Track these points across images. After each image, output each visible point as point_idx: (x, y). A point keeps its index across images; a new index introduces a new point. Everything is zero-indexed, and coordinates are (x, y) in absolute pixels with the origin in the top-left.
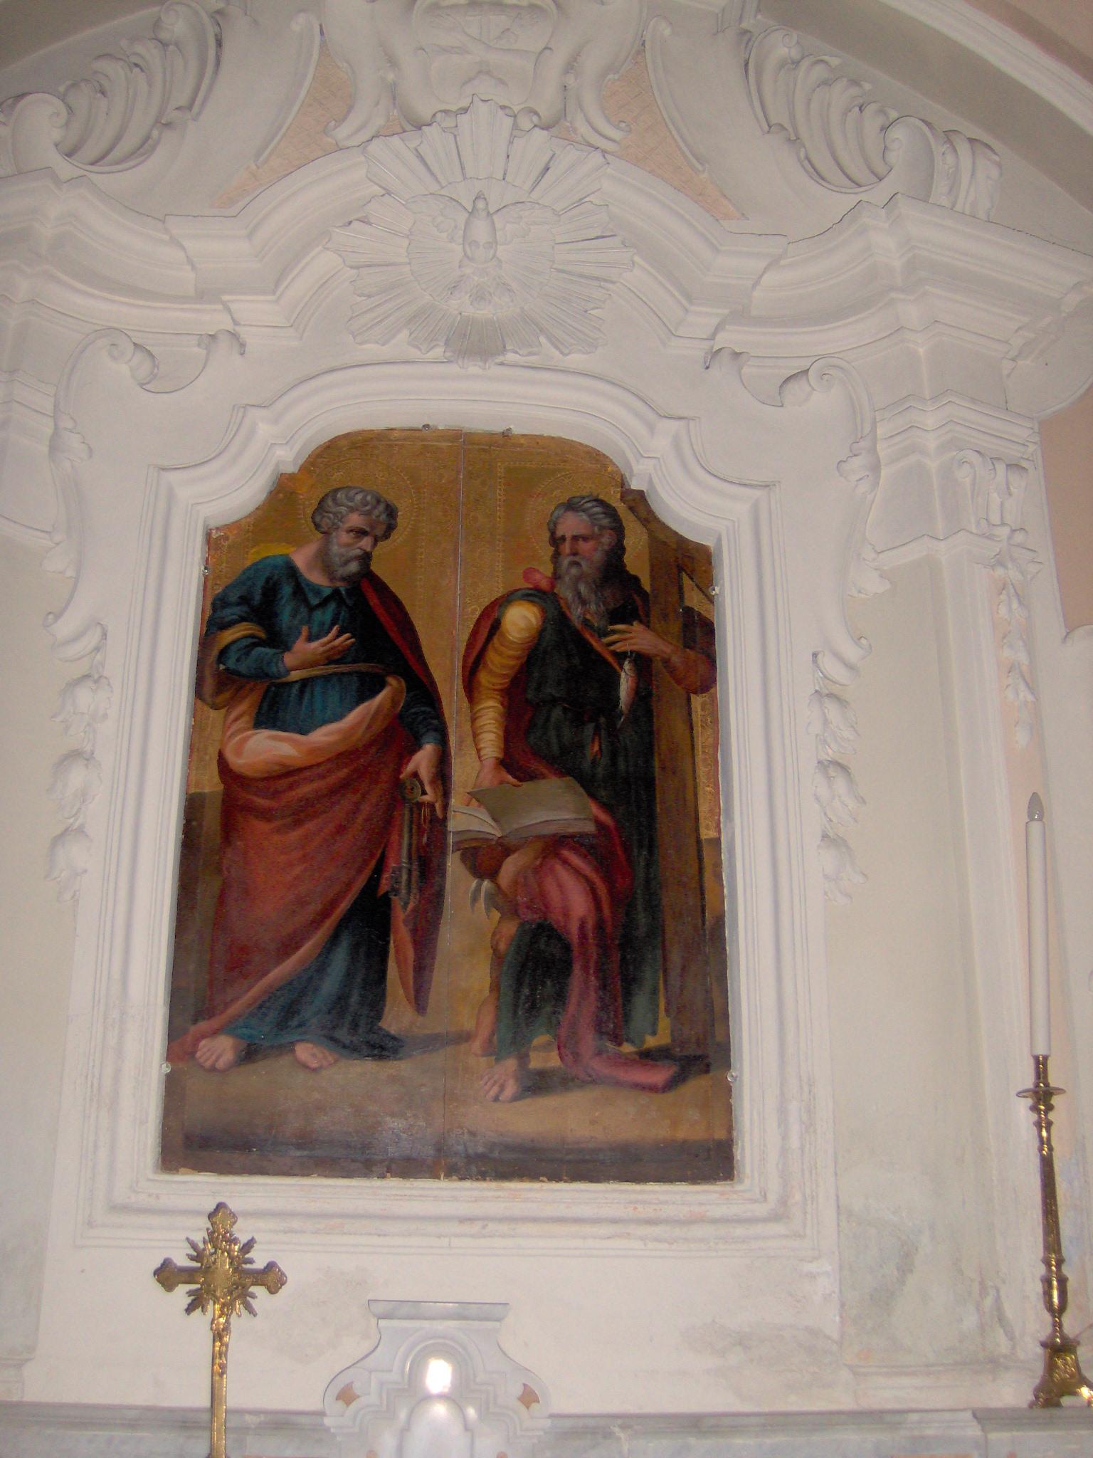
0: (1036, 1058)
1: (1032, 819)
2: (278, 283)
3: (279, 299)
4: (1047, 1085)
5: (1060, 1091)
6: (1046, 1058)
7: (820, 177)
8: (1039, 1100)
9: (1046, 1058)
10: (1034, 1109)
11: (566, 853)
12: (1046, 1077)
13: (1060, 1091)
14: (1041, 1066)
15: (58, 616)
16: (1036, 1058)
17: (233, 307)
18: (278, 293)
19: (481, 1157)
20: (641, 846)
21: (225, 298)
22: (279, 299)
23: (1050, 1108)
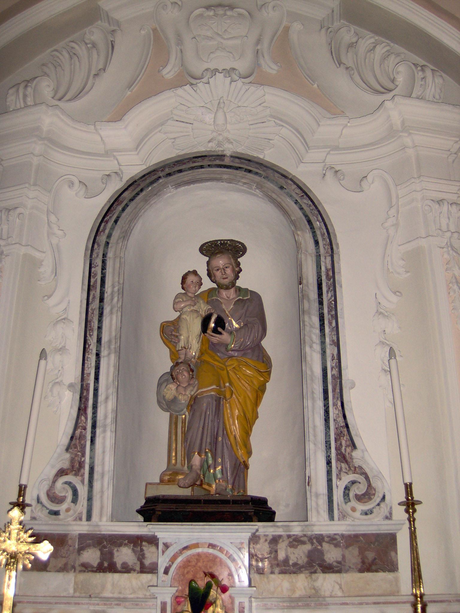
0: (406, 485)
1: (57, 245)
2: (138, 146)
3: (138, 152)
4: (412, 498)
5: (420, 503)
6: (411, 484)
7: (383, 93)
8: (408, 506)
9: (411, 484)
10: (407, 511)
11: (219, 588)
12: (411, 494)
13: (420, 503)
14: (408, 488)
15: (49, 297)
16: (406, 485)
17: (118, 157)
18: (138, 150)
19: (191, 503)
20: (325, 601)
21: (115, 154)
22: (138, 152)
23: (415, 511)
